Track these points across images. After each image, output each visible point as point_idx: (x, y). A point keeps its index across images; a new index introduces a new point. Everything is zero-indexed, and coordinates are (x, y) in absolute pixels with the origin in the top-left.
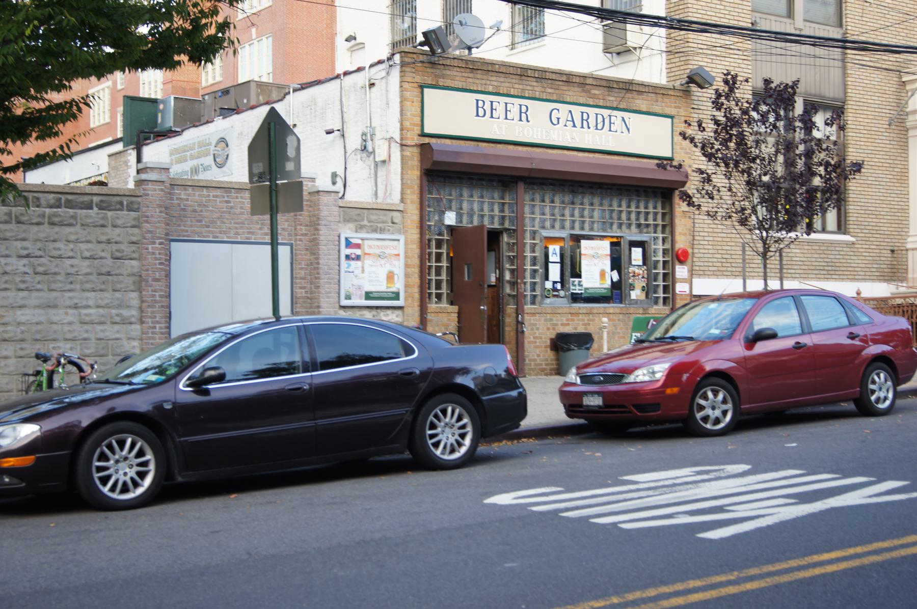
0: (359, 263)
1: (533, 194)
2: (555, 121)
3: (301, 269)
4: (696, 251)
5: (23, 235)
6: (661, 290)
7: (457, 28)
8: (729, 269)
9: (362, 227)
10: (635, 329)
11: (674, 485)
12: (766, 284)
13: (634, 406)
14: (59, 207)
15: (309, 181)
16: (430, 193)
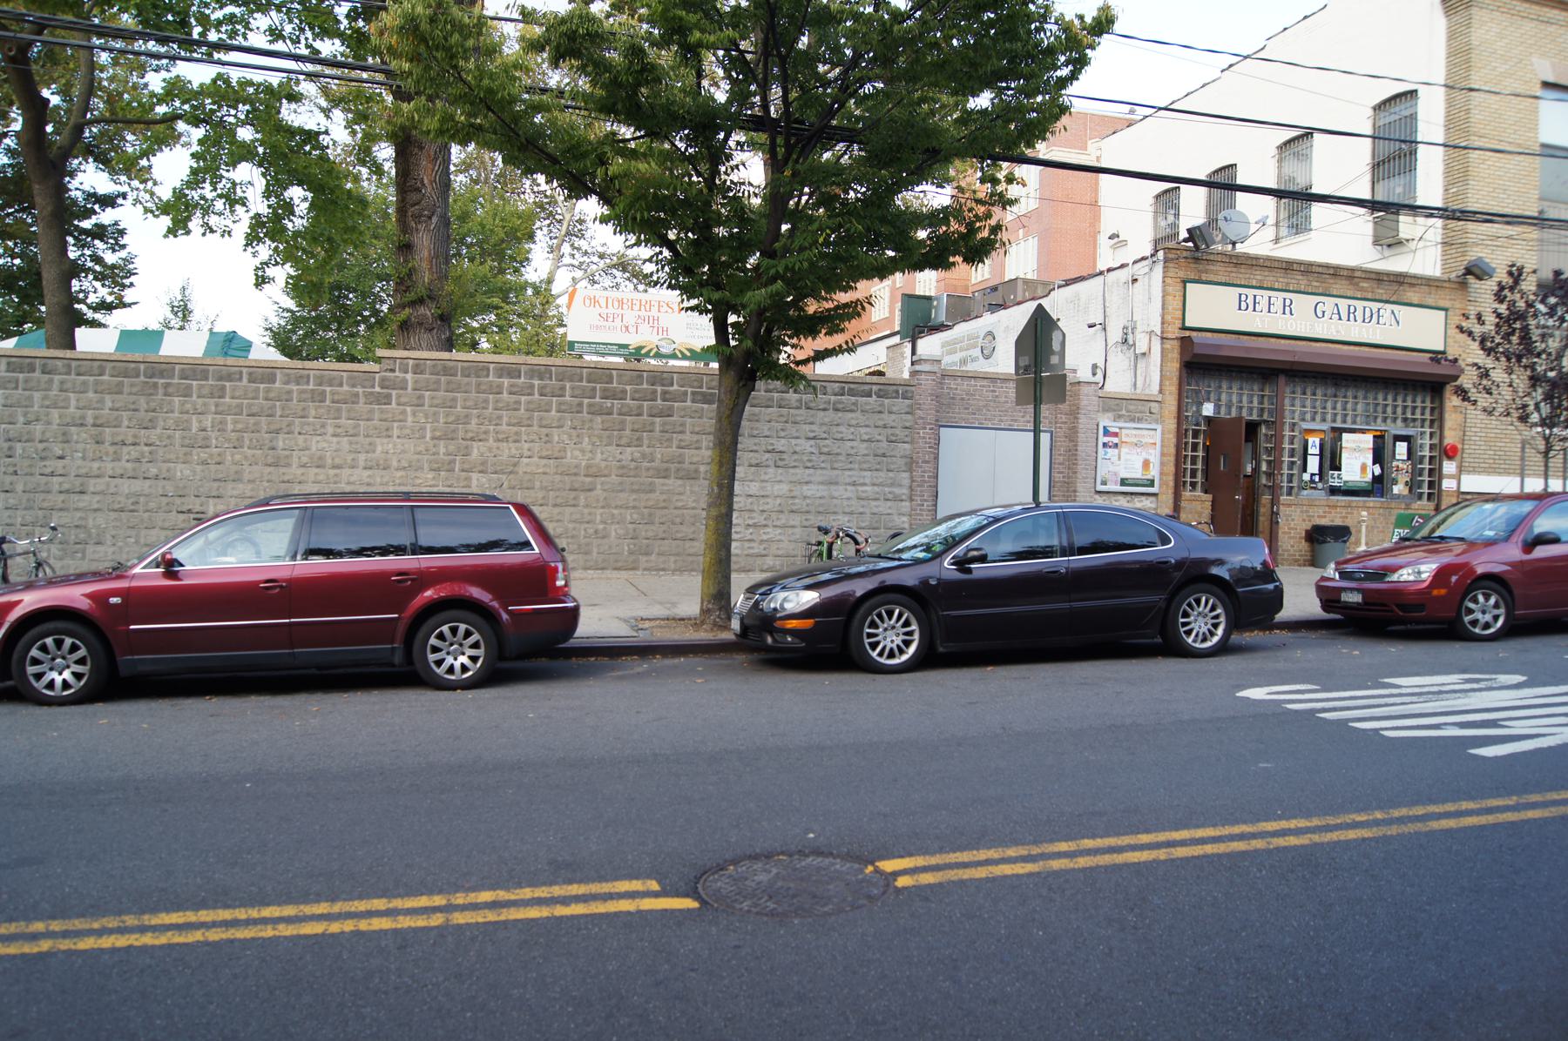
0: (1116, 451)
1: (1294, 386)
2: (1320, 314)
3: (1060, 455)
4: (1466, 447)
5: (812, 420)
6: (1426, 485)
7: (1221, 223)
8: (1502, 466)
9: (1120, 417)
10: (1397, 526)
11: (1440, 692)
12: (1546, 485)
13: (1397, 606)
14: (842, 395)
16: (1189, 384)
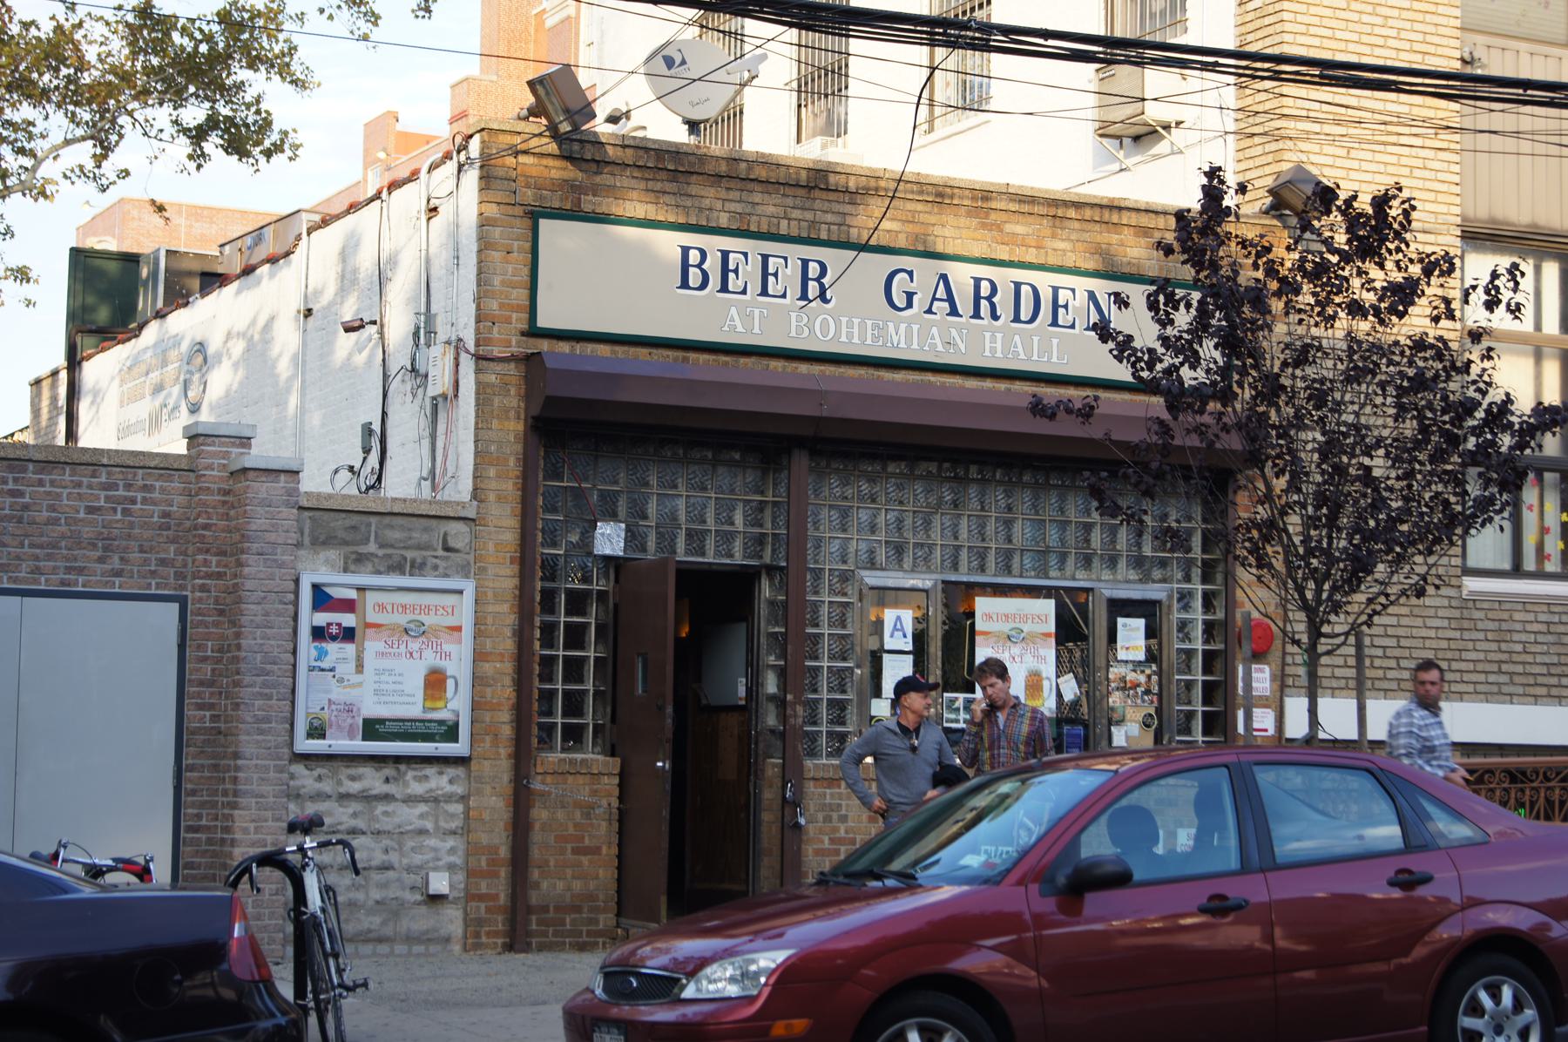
0: (350, 649)
2: (900, 301)
3: (205, 659)
15: (233, 445)
